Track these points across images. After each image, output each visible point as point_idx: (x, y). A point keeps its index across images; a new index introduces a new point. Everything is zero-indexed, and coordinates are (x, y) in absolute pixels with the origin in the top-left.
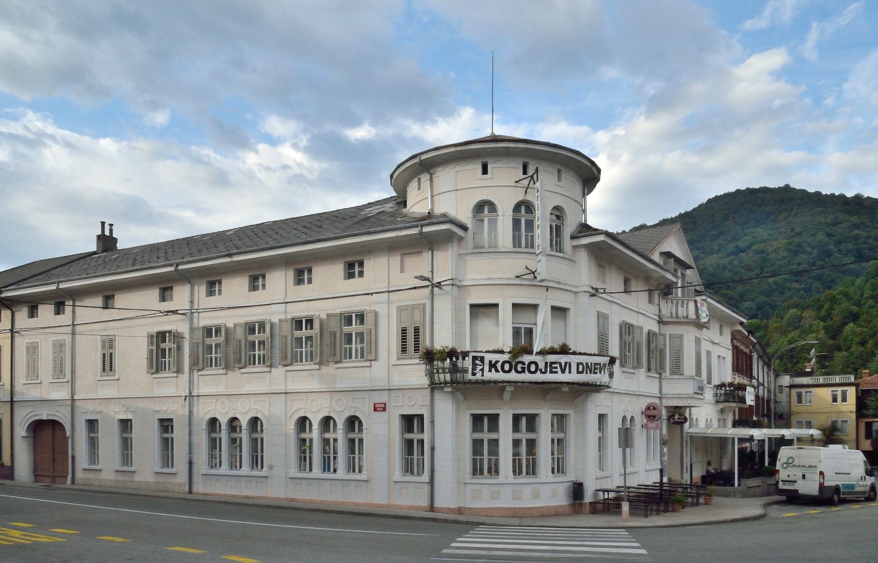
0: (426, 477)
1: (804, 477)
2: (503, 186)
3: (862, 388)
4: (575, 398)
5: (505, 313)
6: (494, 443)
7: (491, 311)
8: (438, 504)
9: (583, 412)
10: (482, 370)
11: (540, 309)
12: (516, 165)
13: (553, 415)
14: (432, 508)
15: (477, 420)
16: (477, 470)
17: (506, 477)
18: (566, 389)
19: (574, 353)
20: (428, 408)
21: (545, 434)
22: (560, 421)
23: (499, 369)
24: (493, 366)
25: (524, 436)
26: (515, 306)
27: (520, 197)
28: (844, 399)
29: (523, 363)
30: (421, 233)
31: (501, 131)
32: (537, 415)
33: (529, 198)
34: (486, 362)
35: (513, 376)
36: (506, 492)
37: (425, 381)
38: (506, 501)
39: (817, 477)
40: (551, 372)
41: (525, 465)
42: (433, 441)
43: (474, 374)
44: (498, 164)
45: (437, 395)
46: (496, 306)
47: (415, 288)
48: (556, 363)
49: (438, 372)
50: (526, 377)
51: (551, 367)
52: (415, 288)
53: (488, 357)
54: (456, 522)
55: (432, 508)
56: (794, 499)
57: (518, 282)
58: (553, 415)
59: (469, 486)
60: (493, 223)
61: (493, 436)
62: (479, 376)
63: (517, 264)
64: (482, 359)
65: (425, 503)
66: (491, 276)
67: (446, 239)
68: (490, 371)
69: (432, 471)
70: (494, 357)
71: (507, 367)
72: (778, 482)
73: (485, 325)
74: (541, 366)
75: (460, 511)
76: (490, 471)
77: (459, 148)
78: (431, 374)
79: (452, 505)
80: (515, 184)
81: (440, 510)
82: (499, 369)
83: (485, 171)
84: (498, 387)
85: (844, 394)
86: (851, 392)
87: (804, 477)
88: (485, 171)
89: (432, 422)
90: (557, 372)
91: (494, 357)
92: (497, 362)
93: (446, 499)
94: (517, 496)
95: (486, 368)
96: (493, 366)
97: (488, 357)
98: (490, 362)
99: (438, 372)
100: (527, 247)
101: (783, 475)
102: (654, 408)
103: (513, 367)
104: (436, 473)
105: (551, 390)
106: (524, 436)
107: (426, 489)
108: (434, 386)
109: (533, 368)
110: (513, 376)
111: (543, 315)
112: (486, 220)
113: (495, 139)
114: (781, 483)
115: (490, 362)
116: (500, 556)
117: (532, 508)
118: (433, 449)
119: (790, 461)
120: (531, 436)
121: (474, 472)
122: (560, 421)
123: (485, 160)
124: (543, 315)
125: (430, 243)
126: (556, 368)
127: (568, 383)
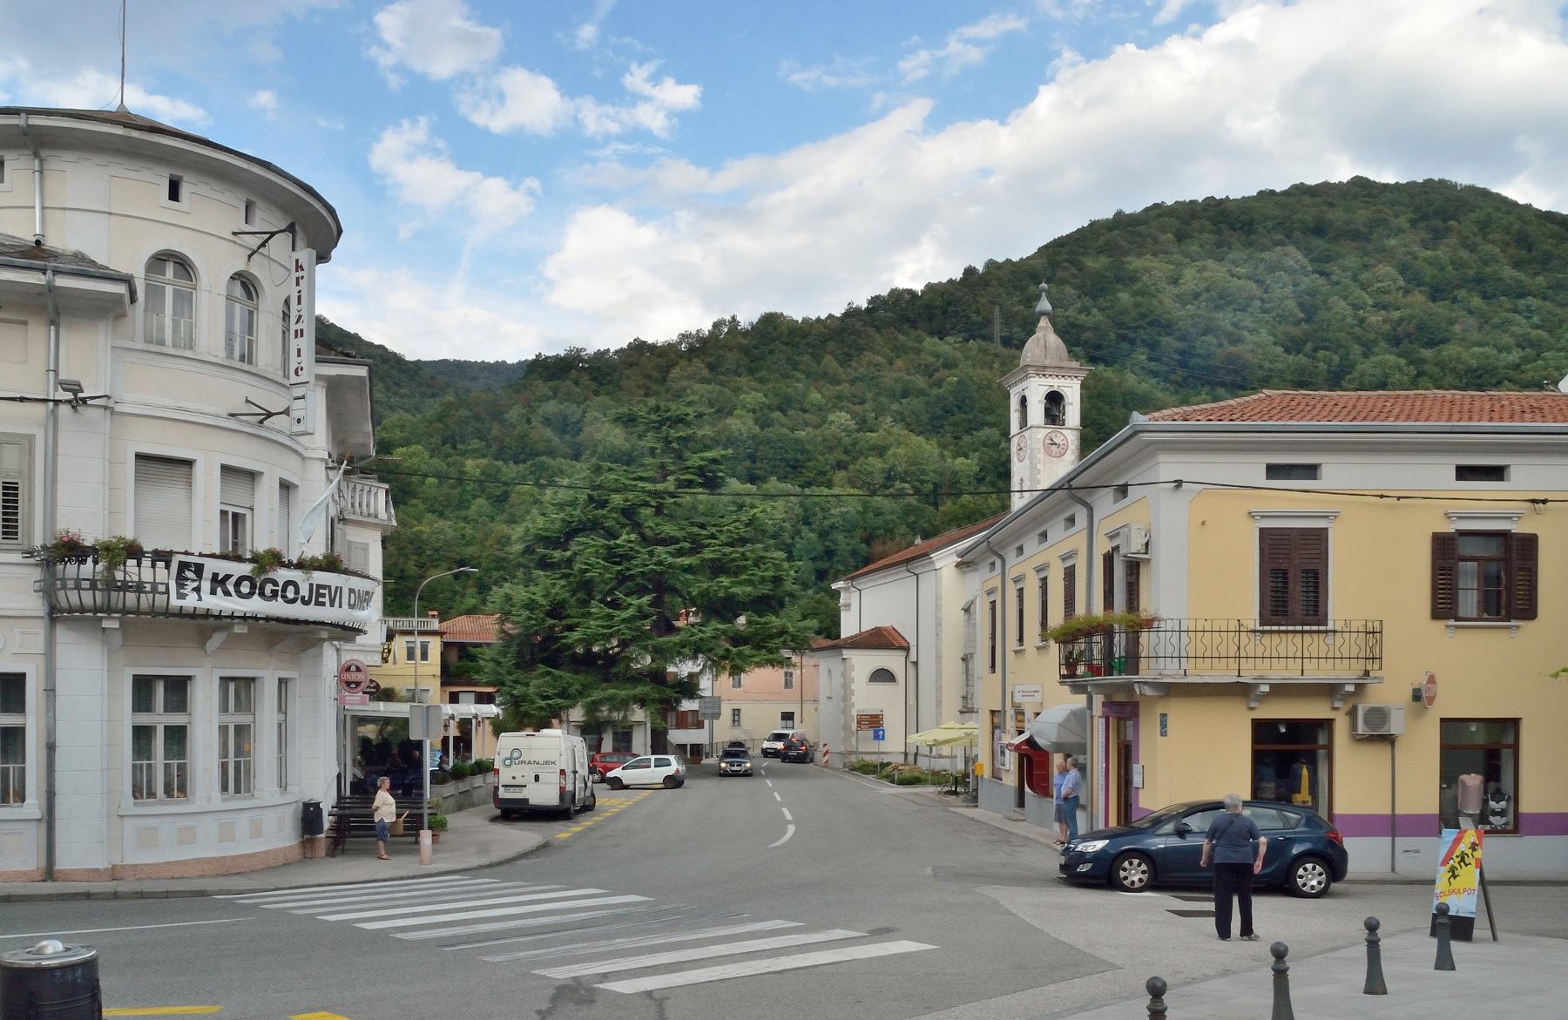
0: (33, 805)
1: (537, 778)
2: (209, 229)
3: (448, 639)
4: (304, 650)
5: (207, 478)
6: (177, 737)
7: (184, 469)
8: (61, 864)
9: (316, 676)
10: (197, 590)
11: (199, 470)
12: (156, 179)
13: (225, 680)
14: (50, 873)
15: (143, 687)
16: (141, 790)
17: (209, 799)
18: (239, 629)
19: (346, 572)
20: (41, 661)
21: (205, 717)
22: (240, 690)
23: (231, 589)
24: (218, 582)
25: (160, 719)
26: (226, 469)
27: (240, 265)
28: (424, 656)
29: (275, 583)
30: (51, 288)
31: (138, 101)
32: (189, 678)
33: (254, 270)
34: (207, 574)
35: (256, 605)
36: (208, 827)
37: (35, 604)
38: (207, 845)
39: (556, 777)
40: (318, 603)
41: (236, 778)
42: (51, 732)
43: (181, 596)
44: (203, 189)
45: (61, 632)
46: (188, 463)
47: (22, 399)
48: (324, 587)
49: (64, 587)
50: (278, 608)
51: (317, 595)
52: (22, 399)
53: (211, 566)
54: (115, 896)
55: (50, 873)
56: (515, 812)
57: (232, 424)
58: (225, 680)
59: (128, 822)
60: (184, 301)
61: (176, 719)
62: (191, 602)
63: (233, 392)
64: (199, 569)
65: (31, 861)
66: (183, 404)
67: (107, 311)
68: (213, 592)
69: (51, 795)
70: (224, 567)
71: (245, 589)
72: (497, 788)
73: (166, 496)
74: (304, 591)
75: (114, 873)
76: (168, 791)
77: (135, 134)
78: (48, 591)
79: (101, 864)
80: (231, 237)
81: (69, 876)
82: (231, 589)
83: (174, 195)
84: (205, 624)
85: (424, 648)
86: (435, 646)
87: (537, 778)
88: (174, 195)
89: (50, 691)
90: (323, 604)
91: (224, 567)
92: (228, 577)
93: (81, 852)
94: (226, 835)
95: (206, 585)
96: (218, 582)
97: (211, 566)
98: (215, 575)
99: (64, 587)
100: (242, 359)
101: (505, 776)
102: (358, 669)
103: (257, 589)
104: (58, 800)
105: (288, 634)
106: (160, 719)
107: (35, 835)
108: (55, 614)
109: (290, 594)
110: (256, 605)
111: (267, 491)
112: (169, 290)
113: (123, 118)
114: (501, 790)
115: (215, 575)
116: (455, 936)
117: (253, 855)
118: (51, 748)
119: (516, 755)
120: (243, 719)
121: (137, 792)
122: (240, 690)
123: (177, 173)
124: (267, 491)
125: (53, 309)
126: (323, 596)
127: (244, 618)
